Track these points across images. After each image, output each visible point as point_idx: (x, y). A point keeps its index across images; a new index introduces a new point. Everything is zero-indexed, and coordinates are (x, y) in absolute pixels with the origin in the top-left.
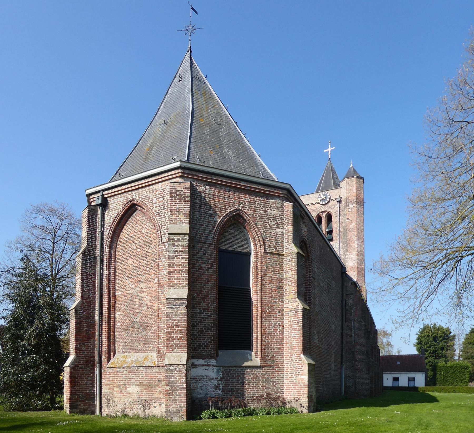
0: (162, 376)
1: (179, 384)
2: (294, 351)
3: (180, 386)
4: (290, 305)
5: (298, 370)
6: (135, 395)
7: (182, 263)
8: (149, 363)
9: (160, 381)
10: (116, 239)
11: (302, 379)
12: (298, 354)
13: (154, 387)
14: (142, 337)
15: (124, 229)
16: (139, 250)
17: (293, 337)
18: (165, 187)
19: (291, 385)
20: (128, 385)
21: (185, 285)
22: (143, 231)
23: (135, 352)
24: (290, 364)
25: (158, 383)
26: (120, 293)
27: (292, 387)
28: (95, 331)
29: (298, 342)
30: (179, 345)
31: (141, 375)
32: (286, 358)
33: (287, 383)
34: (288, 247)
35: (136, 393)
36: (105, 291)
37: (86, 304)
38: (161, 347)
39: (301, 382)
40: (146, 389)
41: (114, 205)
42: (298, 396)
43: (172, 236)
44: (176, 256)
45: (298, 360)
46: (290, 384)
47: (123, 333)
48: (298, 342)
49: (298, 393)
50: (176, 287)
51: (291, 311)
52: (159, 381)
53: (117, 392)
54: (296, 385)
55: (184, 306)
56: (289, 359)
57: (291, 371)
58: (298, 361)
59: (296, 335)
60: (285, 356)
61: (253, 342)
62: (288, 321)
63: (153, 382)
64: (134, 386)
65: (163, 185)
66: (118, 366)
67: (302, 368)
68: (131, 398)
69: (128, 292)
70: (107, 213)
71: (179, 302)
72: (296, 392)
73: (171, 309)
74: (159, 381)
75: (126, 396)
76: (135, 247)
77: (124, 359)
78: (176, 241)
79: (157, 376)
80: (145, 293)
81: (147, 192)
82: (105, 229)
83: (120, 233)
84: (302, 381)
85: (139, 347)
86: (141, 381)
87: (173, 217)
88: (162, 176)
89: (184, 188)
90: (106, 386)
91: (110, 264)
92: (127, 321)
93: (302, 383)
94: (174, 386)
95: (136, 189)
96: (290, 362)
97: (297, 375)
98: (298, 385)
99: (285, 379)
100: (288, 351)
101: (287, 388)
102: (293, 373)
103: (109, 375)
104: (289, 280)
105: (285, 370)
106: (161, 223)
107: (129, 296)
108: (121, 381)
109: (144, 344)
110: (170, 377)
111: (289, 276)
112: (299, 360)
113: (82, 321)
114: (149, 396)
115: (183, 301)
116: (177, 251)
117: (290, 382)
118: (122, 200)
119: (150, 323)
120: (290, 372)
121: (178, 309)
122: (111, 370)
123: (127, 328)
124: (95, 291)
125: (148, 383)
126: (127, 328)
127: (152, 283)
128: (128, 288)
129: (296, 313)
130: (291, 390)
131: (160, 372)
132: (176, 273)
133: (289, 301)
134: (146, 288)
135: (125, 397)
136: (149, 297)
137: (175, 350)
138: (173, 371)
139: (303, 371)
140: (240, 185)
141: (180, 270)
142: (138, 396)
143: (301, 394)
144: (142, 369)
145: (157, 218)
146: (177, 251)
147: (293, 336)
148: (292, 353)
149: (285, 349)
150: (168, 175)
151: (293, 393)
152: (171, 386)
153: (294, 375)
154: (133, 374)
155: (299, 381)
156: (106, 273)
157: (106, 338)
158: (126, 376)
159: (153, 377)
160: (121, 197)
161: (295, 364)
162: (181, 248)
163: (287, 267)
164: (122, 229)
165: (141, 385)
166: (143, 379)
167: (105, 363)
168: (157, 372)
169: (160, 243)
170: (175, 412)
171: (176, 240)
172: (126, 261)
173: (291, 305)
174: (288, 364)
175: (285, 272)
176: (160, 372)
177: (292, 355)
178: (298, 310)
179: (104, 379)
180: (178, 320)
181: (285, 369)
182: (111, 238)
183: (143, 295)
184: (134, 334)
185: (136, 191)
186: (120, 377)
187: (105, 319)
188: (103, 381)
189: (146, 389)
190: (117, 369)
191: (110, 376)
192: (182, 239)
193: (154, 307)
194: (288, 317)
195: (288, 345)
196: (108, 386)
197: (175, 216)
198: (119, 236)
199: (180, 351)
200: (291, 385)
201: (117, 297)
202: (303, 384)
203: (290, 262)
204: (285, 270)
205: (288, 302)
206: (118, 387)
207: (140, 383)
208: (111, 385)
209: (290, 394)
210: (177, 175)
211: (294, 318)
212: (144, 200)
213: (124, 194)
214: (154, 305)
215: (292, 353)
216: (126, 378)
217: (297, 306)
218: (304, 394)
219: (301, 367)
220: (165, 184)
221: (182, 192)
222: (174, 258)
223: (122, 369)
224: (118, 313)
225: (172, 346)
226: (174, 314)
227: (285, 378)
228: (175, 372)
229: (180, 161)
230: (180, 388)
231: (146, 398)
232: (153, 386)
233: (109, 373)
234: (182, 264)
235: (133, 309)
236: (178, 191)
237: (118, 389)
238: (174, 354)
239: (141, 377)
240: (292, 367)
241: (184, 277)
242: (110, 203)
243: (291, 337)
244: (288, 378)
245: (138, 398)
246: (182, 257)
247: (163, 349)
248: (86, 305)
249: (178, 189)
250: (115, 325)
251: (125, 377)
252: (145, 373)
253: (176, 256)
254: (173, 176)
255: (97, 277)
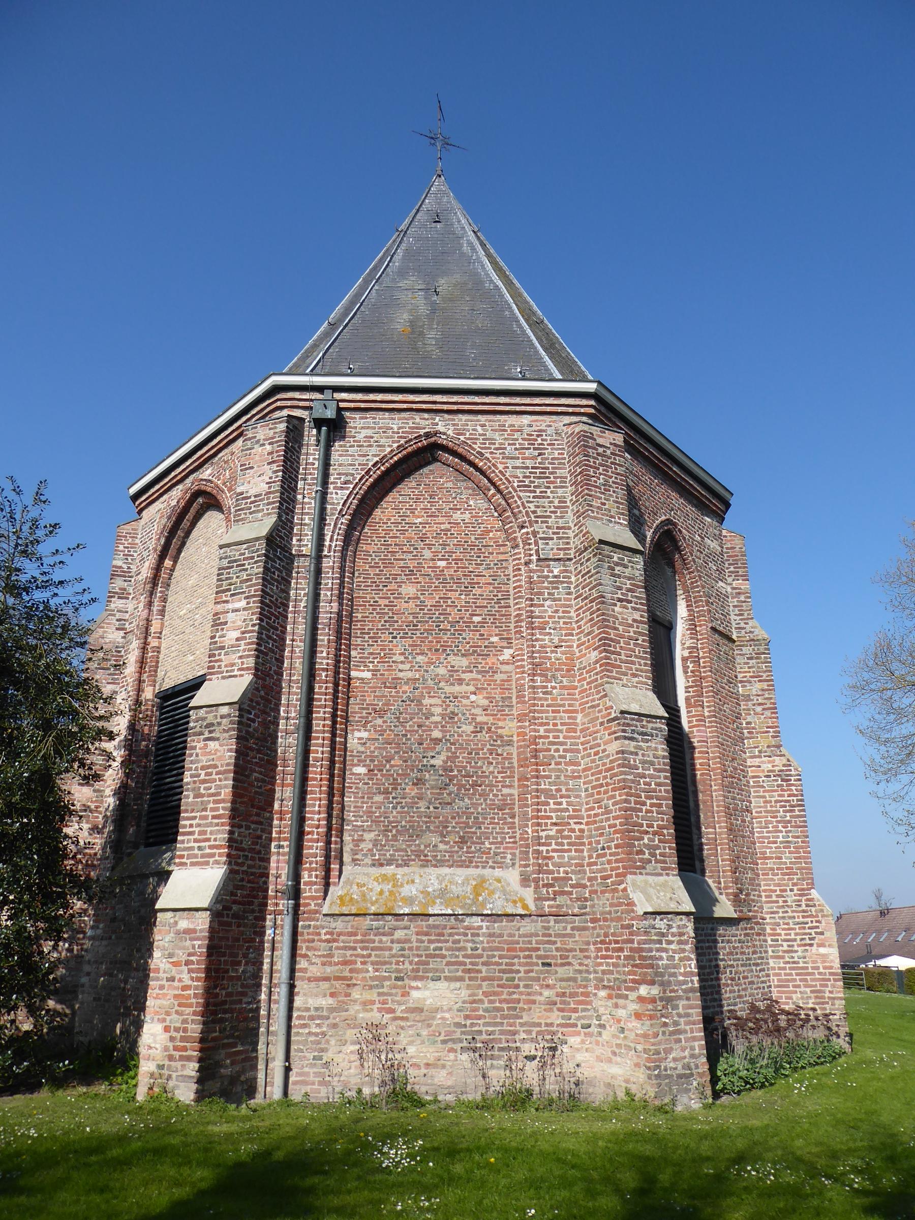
0: (557, 949)
1: (681, 978)
2: (789, 879)
3: (685, 982)
4: (763, 762)
5: (807, 931)
6: (447, 1015)
7: (634, 620)
8: (498, 905)
9: (549, 965)
10: (361, 519)
11: (824, 955)
12: (803, 890)
13: (526, 986)
14: (453, 818)
15: (389, 498)
16: (442, 564)
17: (781, 842)
18: (543, 428)
19: (791, 974)
20: (415, 978)
21: (644, 680)
22: (457, 516)
23: (426, 864)
24: (781, 915)
25: (541, 972)
26: (367, 675)
27: (795, 980)
28: (274, 784)
29: (799, 858)
30: (658, 852)
31: (470, 945)
32: (766, 897)
33: (780, 968)
34: (742, 625)
35: (450, 1009)
36: (324, 659)
37: (262, 693)
38: (547, 851)
39: (821, 966)
40: (495, 994)
41: (365, 433)
42: (818, 1004)
43: (606, 547)
44: (620, 600)
45: (803, 903)
46: (788, 971)
47: (379, 798)
48: (799, 858)
49: (816, 997)
50: (625, 682)
51: (769, 776)
52: (543, 964)
53: (364, 1003)
54: (809, 974)
55: (659, 739)
56: (777, 902)
57: (786, 935)
58: (804, 907)
59: (790, 839)
60: (765, 891)
61: (701, 850)
62: (762, 800)
63: (522, 969)
64: (442, 985)
65: (537, 421)
66: (373, 909)
67: (817, 927)
68: (429, 1026)
69: (401, 675)
70: (341, 446)
71: (650, 725)
72: (809, 994)
73: (633, 744)
74: (543, 964)
75: (406, 1019)
76: (427, 554)
77: (387, 887)
78: (617, 564)
79: (538, 949)
80: (468, 685)
81: (482, 426)
82: (331, 486)
83: (375, 507)
84: (824, 962)
85: (442, 847)
86: (471, 964)
87: (594, 503)
88: (537, 401)
89: (611, 444)
90: (313, 984)
91: (317, 584)
92: (396, 761)
93: (825, 968)
94: (669, 982)
95: (449, 412)
96: (781, 910)
97: (805, 945)
98: (813, 974)
99: (772, 957)
100: (772, 880)
101: (779, 980)
102: (795, 940)
103: (328, 941)
104: (755, 702)
105: (768, 931)
106: (533, 509)
107: (406, 688)
108: (385, 963)
109: (463, 841)
110: (658, 954)
111: (755, 693)
112: (807, 906)
113: (251, 749)
114: (504, 1017)
115: (659, 725)
116: (620, 588)
117: (788, 966)
118: (395, 427)
119: (487, 777)
120: (783, 937)
121: (649, 744)
122: (339, 925)
123: (395, 785)
124: (283, 657)
125: (503, 971)
126: (395, 785)
127: (491, 660)
128: (402, 662)
129: (785, 784)
130: (794, 986)
131: (550, 935)
132: (622, 645)
133: (760, 752)
134: (471, 672)
135: (402, 1023)
136: (481, 697)
137: (649, 868)
138: (663, 935)
139: (822, 933)
140: (671, 469)
141: (630, 638)
142: (457, 1020)
143: (823, 997)
144: (476, 921)
145: (521, 494)
146: (620, 588)
147: (781, 839)
148: (784, 885)
149: (763, 875)
150: (555, 402)
151: (799, 995)
152: (662, 984)
153: (799, 946)
154: (439, 941)
155: (813, 962)
156: (328, 608)
157: (319, 813)
158: (406, 946)
159: (521, 950)
160: (392, 419)
161: (796, 914)
162: (628, 582)
163: (747, 670)
164: (381, 499)
165: (470, 979)
166: (480, 956)
167: (313, 898)
168: (537, 935)
169: (534, 558)
170: (680, 1076)
171: (615, 559)
172: (393, 586)
173: (769, 762)
174: (776, 916)
175: (741, 682)
176: (550, 935)
177: (785, 891)
178: (791, 775)
179: (305, 956)
180: (651, 776)
181: (768, 928)
182: (353, 515)
183: (457, 689)
184: (422, 805)
185: (446, 416)
186: (381, 949)
187: (319, 750)
188: (302, 964)
189: (495, 994)
190: (367, 922)
191: (335, 944)
192: (630, 561)
193: (502, 728)
194: (762, 790)
195: (770, 864)
196: (325, 985)
197: (597, 502)
198: (370, 514)
199: (663, 869)
200: (791, 974)
201: (355, 684)
202: (827, 971)
203: (754, 661)
204: (740, 676)
205: (757, 753)
206: (371, 987)
207: (469, 971)
208: (337, 978)
209: (791, 998)
210: (582, 410)
211: (780, 796)
212: (476, 443)
213: (404, 415)
214: (500, 724)
215: (784, 885)
216: (406, 952)
217: (784, 765)
218: (834, 998)
219: (815, 924)
220: (544, 421)
221: (608, 452)
222: (616, 605)
223: (391, 921)
224: (357, 734)
225: (641, 852)
226: (640, 757)
227: (770, 953)
228: (670, 938)
229: (599, 383)
230: (685, 991)
231: (496, 1024)
232: (521, 984)
233: (331, 934)
234: (635, 625)
235: (419, 726)
236: (601, 446)
237: (373, 995)
238: (651, 879)
239: (469, 952)
240: (788, 924)
241: (641, 658)
242: (351, 425)
243: (775, 842)
244: (780, 954)
245: (458, 1025)
246: (633, 605)
247: (556, 860)
248: (262, 697)
249: (600, 441)
250: (344, 770)
251: (403, 949)
252: (490, 935)
253: (620, 600)
254: (570, 410)
255: (290, 615)
